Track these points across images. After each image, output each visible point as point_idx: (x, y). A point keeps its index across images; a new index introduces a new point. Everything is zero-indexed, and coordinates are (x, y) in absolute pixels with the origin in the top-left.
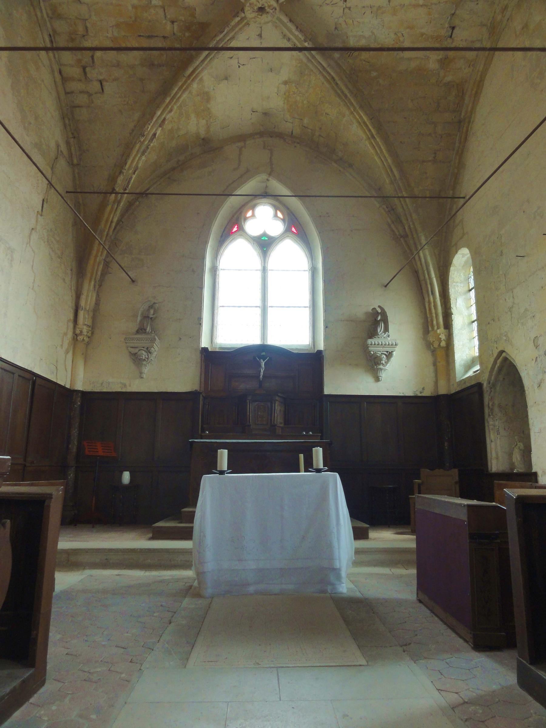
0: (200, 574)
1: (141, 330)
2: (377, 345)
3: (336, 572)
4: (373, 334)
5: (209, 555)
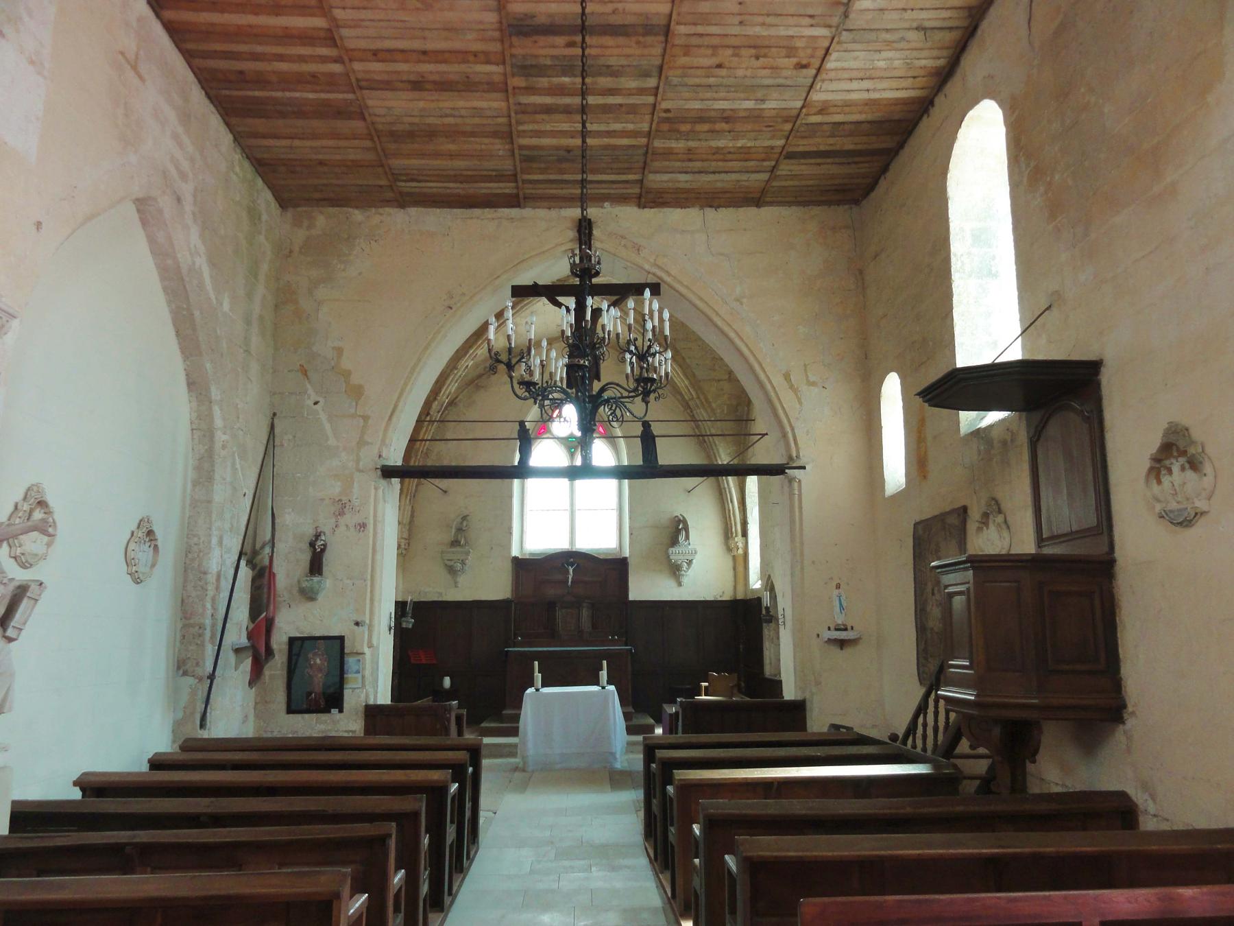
1: (455, 543)
2: (676, 554)
3: (613, 754)
4: (674, 542)
5: (530, 745)
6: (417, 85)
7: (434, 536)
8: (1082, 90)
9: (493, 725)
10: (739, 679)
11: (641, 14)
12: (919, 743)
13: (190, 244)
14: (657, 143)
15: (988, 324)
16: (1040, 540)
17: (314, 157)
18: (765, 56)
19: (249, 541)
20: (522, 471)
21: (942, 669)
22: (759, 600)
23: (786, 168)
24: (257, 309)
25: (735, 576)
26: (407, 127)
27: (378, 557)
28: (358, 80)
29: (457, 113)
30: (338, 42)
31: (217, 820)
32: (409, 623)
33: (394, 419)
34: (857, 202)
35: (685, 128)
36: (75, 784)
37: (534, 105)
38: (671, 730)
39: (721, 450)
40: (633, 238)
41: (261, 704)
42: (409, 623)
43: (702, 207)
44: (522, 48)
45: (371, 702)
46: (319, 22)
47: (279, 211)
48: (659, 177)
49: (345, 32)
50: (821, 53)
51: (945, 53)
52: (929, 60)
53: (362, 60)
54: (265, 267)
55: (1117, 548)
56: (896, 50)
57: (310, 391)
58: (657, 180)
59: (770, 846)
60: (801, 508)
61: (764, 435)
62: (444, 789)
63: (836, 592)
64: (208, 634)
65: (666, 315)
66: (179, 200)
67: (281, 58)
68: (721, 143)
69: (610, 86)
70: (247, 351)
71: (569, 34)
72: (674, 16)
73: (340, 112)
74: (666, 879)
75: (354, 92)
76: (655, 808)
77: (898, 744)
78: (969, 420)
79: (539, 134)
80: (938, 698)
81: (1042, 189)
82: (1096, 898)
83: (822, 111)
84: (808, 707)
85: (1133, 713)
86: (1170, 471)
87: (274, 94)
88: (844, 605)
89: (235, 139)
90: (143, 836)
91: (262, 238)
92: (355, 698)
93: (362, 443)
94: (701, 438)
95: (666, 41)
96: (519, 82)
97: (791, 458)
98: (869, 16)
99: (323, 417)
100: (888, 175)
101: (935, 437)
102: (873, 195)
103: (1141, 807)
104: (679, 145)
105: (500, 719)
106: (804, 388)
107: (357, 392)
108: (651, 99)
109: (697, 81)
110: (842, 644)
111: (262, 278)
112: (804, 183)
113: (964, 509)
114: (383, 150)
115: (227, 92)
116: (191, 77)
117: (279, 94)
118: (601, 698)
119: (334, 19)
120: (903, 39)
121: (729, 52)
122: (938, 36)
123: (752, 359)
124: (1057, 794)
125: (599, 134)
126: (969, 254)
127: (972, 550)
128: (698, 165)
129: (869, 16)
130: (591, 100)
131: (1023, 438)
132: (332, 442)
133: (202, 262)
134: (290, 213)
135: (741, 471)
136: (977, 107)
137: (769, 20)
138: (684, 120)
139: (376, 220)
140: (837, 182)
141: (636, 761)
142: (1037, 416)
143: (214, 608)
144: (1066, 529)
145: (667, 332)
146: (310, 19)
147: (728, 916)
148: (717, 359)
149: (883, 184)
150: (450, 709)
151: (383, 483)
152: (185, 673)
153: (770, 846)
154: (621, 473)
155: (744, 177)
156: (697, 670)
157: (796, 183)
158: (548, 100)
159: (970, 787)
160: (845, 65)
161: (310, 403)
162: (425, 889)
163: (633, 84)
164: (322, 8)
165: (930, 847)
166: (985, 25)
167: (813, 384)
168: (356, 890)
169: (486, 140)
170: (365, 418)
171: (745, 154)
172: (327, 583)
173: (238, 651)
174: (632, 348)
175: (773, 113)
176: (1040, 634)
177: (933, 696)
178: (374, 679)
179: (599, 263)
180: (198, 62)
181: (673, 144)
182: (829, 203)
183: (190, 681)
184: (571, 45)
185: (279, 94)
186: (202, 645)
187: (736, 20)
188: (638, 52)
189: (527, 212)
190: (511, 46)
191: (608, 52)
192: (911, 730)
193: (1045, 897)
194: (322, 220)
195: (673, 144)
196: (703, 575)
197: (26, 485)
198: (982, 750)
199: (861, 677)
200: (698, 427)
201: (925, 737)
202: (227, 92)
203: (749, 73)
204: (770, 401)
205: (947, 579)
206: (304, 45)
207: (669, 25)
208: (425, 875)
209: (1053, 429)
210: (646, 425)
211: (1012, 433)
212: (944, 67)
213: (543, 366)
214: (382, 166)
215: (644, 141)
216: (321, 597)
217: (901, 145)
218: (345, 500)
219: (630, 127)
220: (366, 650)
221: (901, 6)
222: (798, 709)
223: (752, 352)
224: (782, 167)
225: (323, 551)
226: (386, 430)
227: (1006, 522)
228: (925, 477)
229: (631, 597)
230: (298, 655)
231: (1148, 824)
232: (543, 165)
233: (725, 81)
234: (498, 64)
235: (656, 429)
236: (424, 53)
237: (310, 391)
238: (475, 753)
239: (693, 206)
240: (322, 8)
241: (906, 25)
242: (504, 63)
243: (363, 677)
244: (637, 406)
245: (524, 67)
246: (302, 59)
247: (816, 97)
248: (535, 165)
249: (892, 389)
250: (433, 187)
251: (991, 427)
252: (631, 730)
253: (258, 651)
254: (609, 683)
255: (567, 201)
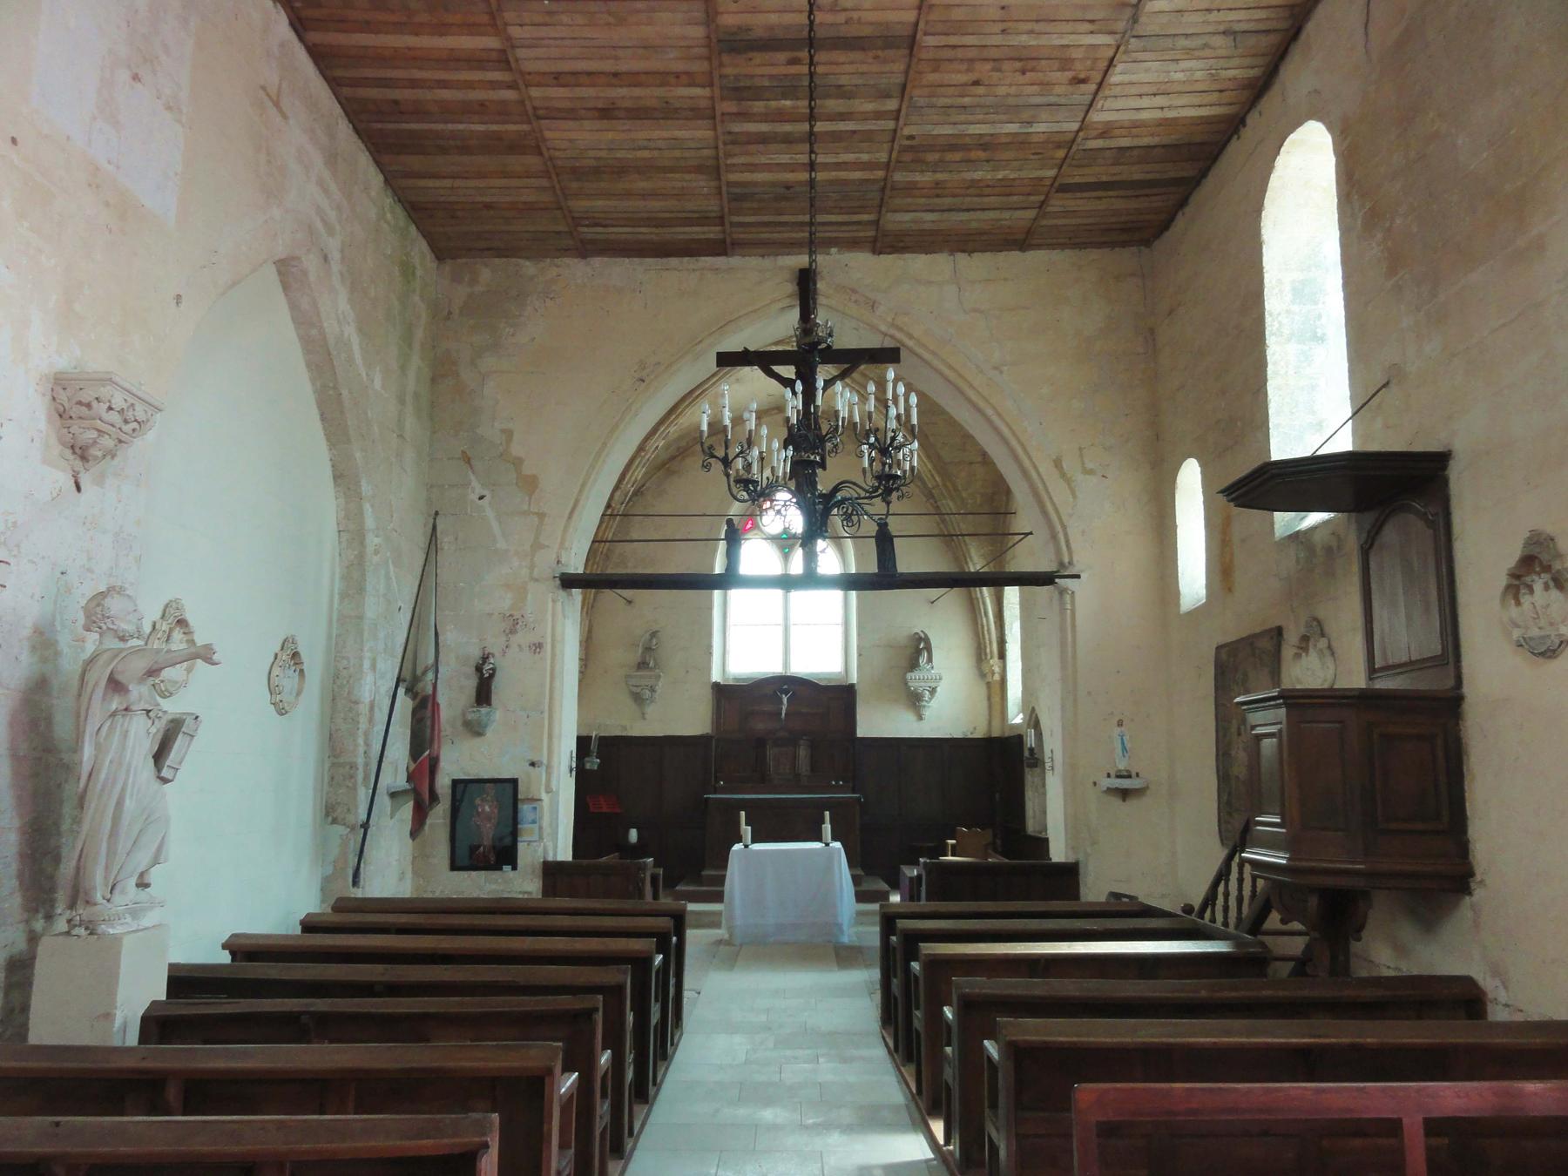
0: (730, 929)
1: (642, 665)
2: (916, 679)
3: (840, 926)
4: (913, 665)
5: (738, 912)
6: (606, 113)
7: (619, 657)
8: (1431, 115)
9: (691, 888)
10: (995, 836)
11: (880, 24)
12: (1219, 917)
13: (338, 311)
14: (898, 177)
15: (1311, 405)
16: (1372, 671)
17: (479, 199)
18: (1032, 70)
19: (408, 665)
20: (728, 580)
21: (1247, 828)
22: (1019, 739)
23: (1058, 203)
24: (411, 385)
25: (990, 707)
26: (593, 163)
27: (557, 684)
28: (535, 108)
29: (652, 145)
30: (513, 65)
31: (393, 990)
32: (593, 763)
33: (575, 517)
34: (1147, 243)
35: (932, 157)
36: (224, 947)
37: (748, 134)
38: (912, 896)
39: (973, 552)
40: (868, 293)
41: (420, 861)
42: (593, 763)
43: (952, 252)
44: (734, 67)
45: (550, 858)
46: (492, 42)
47: (435, 265)
48: (899, 217)
49: (521, 53)
50: (1103, 65)
51: (1260, 61)
52: (1238, 70)
53: (539, 85)
54: (419, 334)
55: (1465, 682)
56: (1199, 58)
57: (475, 483)
58: (898, 220)
59: (1035, 1030)
60: (1074, 626)
61: (1027, 534)
62: (650, 960)
63: (1117, 730)
64: (360, 776)
65: (914, 399)
66: (326, 258)
67: (444, 84)
68: (978, 175)
69: (842, 109)
70: (400, 436)
71: (792, 49)
72: (921, 25)
73: (516, 147)
74: (909, 1072)
75: (529, 122)
76: (896, 983)
77: (1193, 917)
78: (1286, 522)
79: (753, 168)
80: (1243, 861)
81: (1379, 236)
82: (1419, 1090)
83: (1104, 134)
84: (1082, 871)
85: (1481, 882)
86: (1531, 590)
87: (434, 126)
88: (1128, 746)
89: (386, 181)
90: (320, 1005)
91: (417, 298)
92: (531, 853)
93: (537, 546)
94: (949, 538)
95: (911, 55)
96: (730, 107)
97: (1062, 564)
98: (1164, 19)
99: (490, 514)
100: (1187, 210)
101: (1243, 541)
102: (1167, 234)
103: (1490, 996)
104: (925, 178)
105: (698, 880)
106: (1079, 477)
107: (530, 484)
108: (891, 124)
109: (948, 101)
110: (1124, 794)
111: (417, 346)
112: (1079, 221)
113: (1279, 631)
114: (562, 189)
115: (379, 126)
116: (338, 110)
117: (440, 127)
118: (823, 858)
119: (509, 39)
120: (1206, 46)
121: (988, 66)
122: (1252, 40)
123: (1014, 443)
124: (1387, 978)
125: (826, 167)
126: (1288, 312)
127: (1287, 683)
128: (948, 201)
129: (1164, 19)
130: (820, 127)
131: (1352, 542)
132: (501, 544)
133: (351, 331)
134: (448, 266)
135: (998, 581)
136: (1300, 130)
137: (1038, 27)
138: (931, 148)
139: (554, 272)
140: (1123, 219)
141: (871, 935)
142: (1369, 518)
143: (367, 744)
144: (1405, 659)
145: (915, 421)
146: (484, 38)
147: (987, 1111)
148: (967, 437)
149: (1180, 222)
150: (643, 868)
151: (562, 594)
152: (334, 821)
153: (1035, 1030)
154: (850, 582)
155: (1007, 215)
156: (942, 826)
157: (1073, 221)
158: (764, 127)
159: (1284, 969)
160: (1134, 78)
161: (475, 497)
162: (630, 1075)
163: (869, 107)
164: (494, 25)
165: (1228, 1033)
166: (1310, 27)
167: (1091, 472)
168: (568, 1068)
169: (687, 177)
170: (541, 516)
171: (1006, 188)
172: (496, 716)
173: (393, 795)
174: (872, 440)
175: (1042, 138)
176: (1374, 789)
177: (1236, 859)
178: (553, 832)
179: (830, 335)
180: (346, 91)
181: (918, 177)
182: (1112, 245)
183: (340, 830)
184: (793, 62)
185: (440, 127)
186: (355, 788)
187: (998, 27)
188: (875, 68)
189: (735, 261)
190: (721, 65)
191: (837, 69)
192: (1210, 899)
193: (1358, 1089)
194: (488, 273)
195: (918, 177)
196: (947, 708)
197: (169, 597)
198: (1296, 926)
199: (1146, 835)
200: (943, 521)
201: (1226, 909)
202: (379, 126)
203: (1013, 90)
204: (1036, 494)
205: (1255, 717)
206: (471, 69)
207: (914, 36)
208: (630, 1058)
209: (1390, 534)
210: (883, 527)
211: (1339, 537)
212: (1257, 79)
213: (762, 459)
214: (560, 208)
215: (880, 174)
216: (490, 733)
217: (1204, 174)
218: (517, 615)
219: (865, 157)
220: (544, 796)
221: (1205, 6)
222: (1070, 872)
223: (1014, 433)
224: (1052, 202)
225: (492, 676)
226: (565, 530)
227: (1329, 647)
228: (1230, 590)
229: (860, 733)
230: (461, 801)
231: (1497, 1014)
232: (755, 205)
233: (982, 101)
234: (703, 86)
235: (894, 526)
236: (616, 75)
237: (475, 483)
238: (679, 921)
239: (940, 251)
240: (495, 25)
241: (1210, 29)
242: (711, 85)
243: (541, 828)
244: (878, 506)
245: (736, 89)
246: (470, 85)
247: (1096, 117)
248: (747, 205)
249: (1190, 479)
250: (622, 232)
251: (1313, 529)
252: (861, 897)
253: (420, 793)
254: (834, 839)
255: (790, 247)
